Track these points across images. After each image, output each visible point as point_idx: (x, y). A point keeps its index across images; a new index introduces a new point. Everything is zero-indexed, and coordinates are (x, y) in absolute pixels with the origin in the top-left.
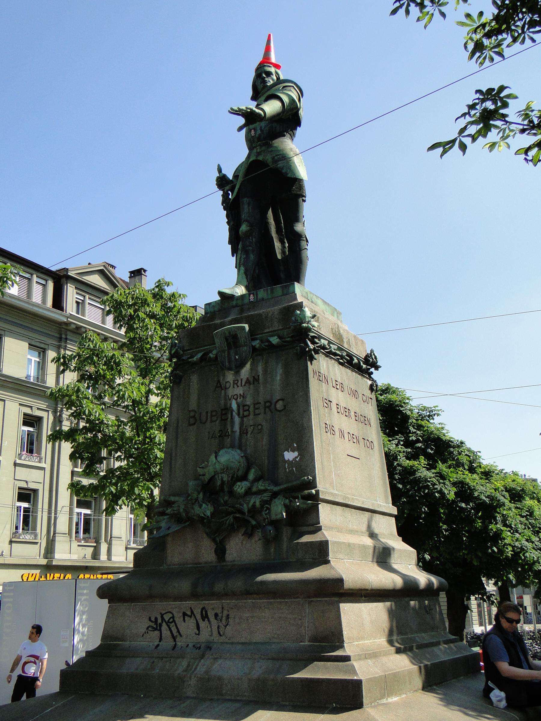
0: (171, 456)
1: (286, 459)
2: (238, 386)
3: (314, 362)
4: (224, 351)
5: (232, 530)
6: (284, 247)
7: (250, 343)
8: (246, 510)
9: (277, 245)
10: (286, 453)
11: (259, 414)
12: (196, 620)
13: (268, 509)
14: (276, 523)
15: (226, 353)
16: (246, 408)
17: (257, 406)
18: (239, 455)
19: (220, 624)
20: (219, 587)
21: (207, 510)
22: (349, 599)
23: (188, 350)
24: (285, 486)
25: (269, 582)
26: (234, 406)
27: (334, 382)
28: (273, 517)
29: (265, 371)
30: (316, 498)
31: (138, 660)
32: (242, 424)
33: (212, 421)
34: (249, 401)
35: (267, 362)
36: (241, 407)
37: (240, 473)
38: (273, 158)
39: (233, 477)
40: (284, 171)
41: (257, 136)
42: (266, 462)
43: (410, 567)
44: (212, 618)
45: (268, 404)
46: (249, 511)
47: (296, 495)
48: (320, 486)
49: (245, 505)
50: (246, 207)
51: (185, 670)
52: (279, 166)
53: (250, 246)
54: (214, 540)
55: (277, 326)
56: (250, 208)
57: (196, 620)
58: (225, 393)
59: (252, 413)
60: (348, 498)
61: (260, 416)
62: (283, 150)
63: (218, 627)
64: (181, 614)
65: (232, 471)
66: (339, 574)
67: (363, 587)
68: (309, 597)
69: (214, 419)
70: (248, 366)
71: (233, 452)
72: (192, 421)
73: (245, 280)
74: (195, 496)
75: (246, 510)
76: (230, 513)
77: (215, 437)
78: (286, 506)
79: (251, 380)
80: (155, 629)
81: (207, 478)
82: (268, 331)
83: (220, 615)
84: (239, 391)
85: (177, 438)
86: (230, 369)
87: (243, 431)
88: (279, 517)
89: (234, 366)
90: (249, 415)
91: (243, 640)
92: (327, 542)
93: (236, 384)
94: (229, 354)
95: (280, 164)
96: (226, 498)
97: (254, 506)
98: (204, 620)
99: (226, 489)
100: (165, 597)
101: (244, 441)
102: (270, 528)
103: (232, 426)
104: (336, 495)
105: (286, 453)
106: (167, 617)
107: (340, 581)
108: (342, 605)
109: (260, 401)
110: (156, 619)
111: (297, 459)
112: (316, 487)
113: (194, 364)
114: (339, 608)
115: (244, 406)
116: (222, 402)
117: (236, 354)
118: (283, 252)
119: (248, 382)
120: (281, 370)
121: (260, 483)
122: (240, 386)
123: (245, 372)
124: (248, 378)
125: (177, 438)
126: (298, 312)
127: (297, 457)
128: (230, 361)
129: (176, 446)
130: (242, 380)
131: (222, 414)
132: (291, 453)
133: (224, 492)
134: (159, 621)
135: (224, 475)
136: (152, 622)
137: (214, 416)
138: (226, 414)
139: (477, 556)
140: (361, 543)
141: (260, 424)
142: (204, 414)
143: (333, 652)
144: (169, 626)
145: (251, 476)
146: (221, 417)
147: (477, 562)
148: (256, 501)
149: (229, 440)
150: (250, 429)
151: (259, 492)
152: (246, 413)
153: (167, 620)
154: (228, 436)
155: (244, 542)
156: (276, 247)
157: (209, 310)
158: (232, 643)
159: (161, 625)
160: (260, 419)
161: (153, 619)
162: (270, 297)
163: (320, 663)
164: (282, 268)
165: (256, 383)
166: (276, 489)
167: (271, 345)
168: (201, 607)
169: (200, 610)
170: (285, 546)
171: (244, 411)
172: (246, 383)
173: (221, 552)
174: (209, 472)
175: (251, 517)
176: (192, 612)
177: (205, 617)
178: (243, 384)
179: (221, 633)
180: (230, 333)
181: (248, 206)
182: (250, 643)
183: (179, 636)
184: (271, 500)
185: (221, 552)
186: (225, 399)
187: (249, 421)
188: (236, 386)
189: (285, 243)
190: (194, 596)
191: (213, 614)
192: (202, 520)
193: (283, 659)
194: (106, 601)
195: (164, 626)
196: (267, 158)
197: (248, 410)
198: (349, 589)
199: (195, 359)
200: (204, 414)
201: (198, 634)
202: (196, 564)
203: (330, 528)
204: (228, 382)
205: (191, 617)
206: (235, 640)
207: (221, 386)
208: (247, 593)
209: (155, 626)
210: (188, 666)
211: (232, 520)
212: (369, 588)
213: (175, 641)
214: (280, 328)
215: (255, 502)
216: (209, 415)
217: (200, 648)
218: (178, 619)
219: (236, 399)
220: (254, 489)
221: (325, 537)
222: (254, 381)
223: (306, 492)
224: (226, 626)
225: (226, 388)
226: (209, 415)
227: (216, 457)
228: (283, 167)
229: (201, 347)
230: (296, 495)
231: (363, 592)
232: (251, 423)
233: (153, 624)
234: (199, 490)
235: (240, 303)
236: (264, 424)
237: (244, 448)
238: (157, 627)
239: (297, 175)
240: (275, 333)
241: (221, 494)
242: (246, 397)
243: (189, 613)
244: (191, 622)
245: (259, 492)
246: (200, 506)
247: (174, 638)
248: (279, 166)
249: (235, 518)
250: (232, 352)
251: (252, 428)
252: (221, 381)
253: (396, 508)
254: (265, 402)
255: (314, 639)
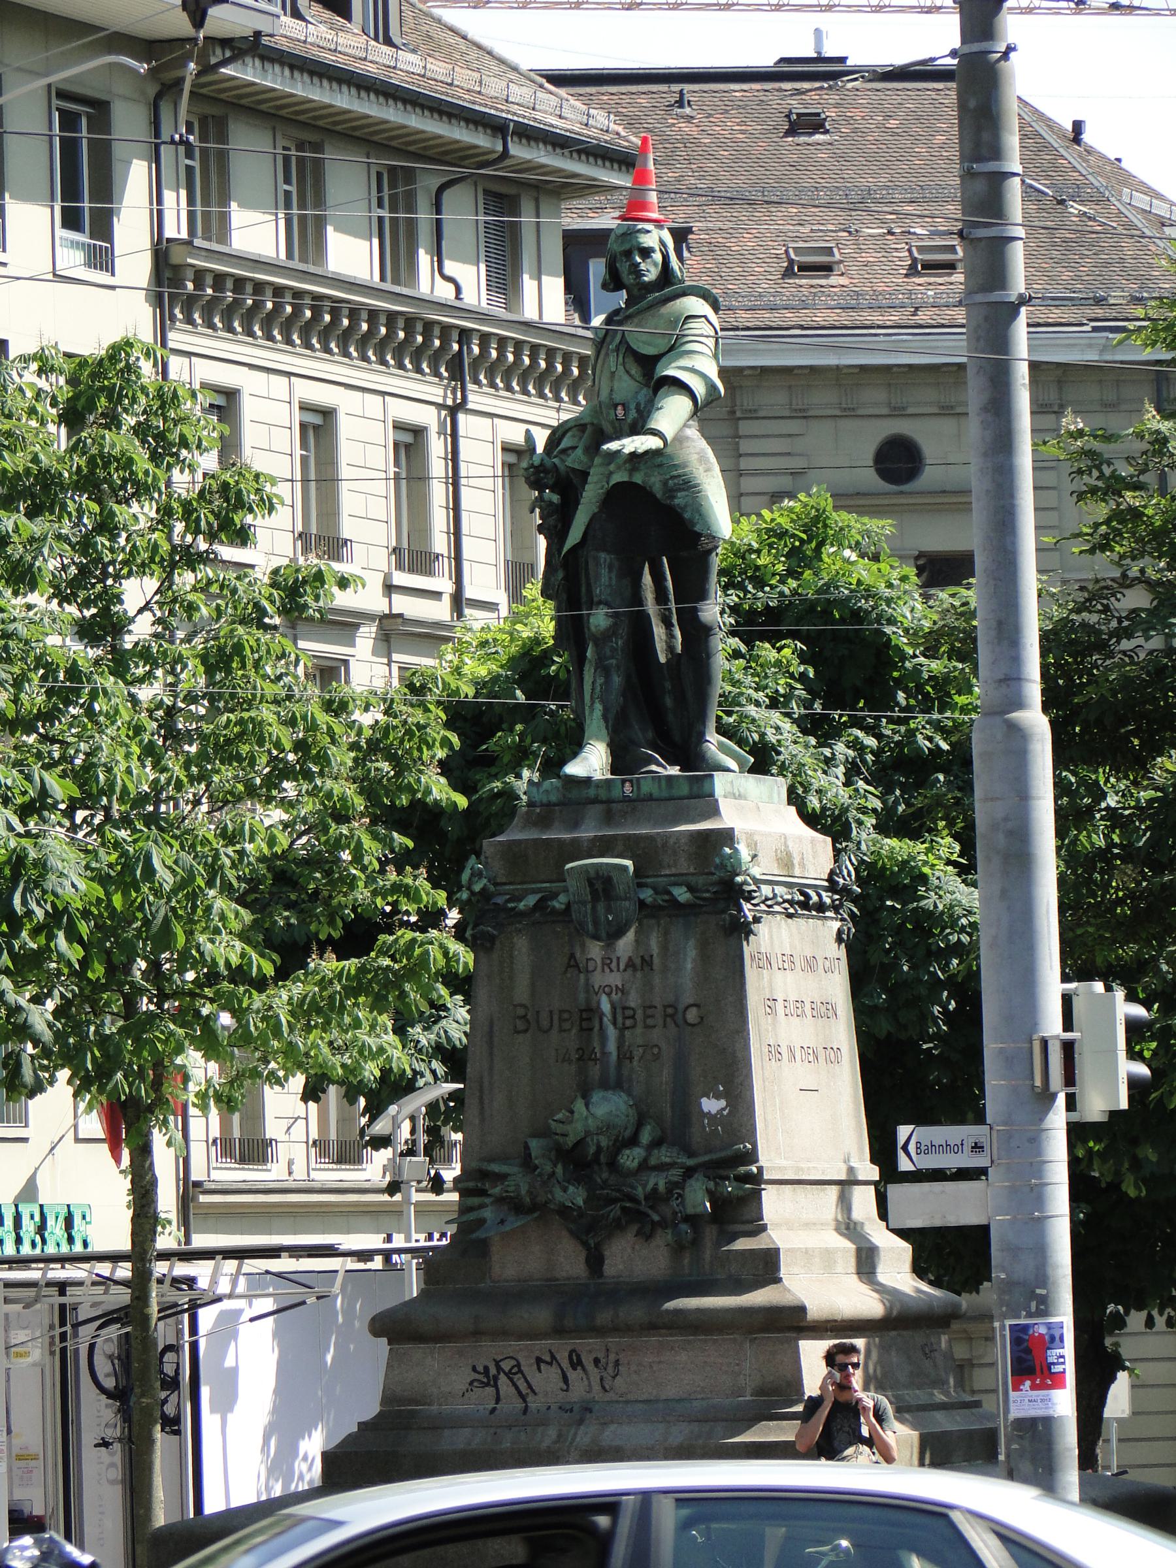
0: (481, 1087)
1: (706, 1110)
2: (611, 971)
3: (752, 938)
4: (584, 903)
5: (618, 1226)
6: (671, 636)
7: (636, 893)
8: (641, 1196)
9: (659, 631)
10: (704, 1101)
11: (654, 1027)
12: (562, 1370)
13: (680, 1195)
14: (694, 1220)
15: (589, 906)
16: (629, 1013)
17: (649, 1012)
18: (625, 1102)
19: (605, 1374)
20: (604, 1317)
21: (577, 1196)
22: (814, 1334)
23: (505, 884)
24: (706, 1158)
25: (689, 1310)
26: (606, 1006)
27: (779, 956)
28: (690, 1211)
29: (664, 948)
30: (757, 1179)
31: (467, 1431)
32: (621, 1040)
33: (561, 1030)
34: (633, 1001)
35: (666, 933)
36: (619, 1011)
37: (628, 1133)
38: (665, 483)
39: (616, 1140)
40: (687, 515)
41: (629, 421)
42: (669, 1114)
43: (899, 1276)
44: (590, 1367)
45: (670, 1011)
46: (646, 1198)
47: (723, 1173)
48: (764, 1159)
49: (640, 1189)
50: (604, 572)
51: (555, 1442)
52: (676, 501)
53: (612, 657)
54: (585, 1244)
55: (684, 866)
56: (613, 576)
57: (562, 1370)
58: (587, 980)
59: (640, 1025)
60: (802, 1169)
61: (656, 1031)
62: (684, 465)
63: (602, 1379)
64: (533, 1361)
65: (615, 1132)
66: (799, 1299)
67: (831, 1318)
68: (751, 1333)
69: (566, 1026)
70: (630, 935)
71: (615, 1098)
72: (521, 1025)
73: (604, 732)
74: (548, 1168)
75: (641, 1196)
76: (614, 1201)
77: (570, 1061)
78: (709, 1191)
79: (638, 961)
80: (487, 1384)
81: (570, 1141)
82: (667, 872)
83: (603, 1361)
84: (614, 979)
85: (491, 1054)
86: (596, 937)
87: (625, 1055)
88: (699, 1210)
89: (604, 935)
90: (634, 1027)
91: (644, 1397)
92: (777, 1250)
93: (609, 965)
94: (594, 909)
95: (680, 500)
96: (605, 1175)
97: (655, 1189)
98: (575, 1369)
99: (603, 1159)
100: (503, 1334)
101: (625, 1072)
102: (684, 1227)
103: (603, 1043)
104: (785, 1168)
105: (704, 1101)
106: (506, 1365)
107: (801, 1310)
108: (802, 1343)
109: (654, 1003)
110: (486, 1368)
111: (725, 1113)
112: (757, 1161)
113: (522, 914)
114: (797, 1347)
115: (624, 1008)
116: (582, 996)
117: (609, 910)
118: (670, 648)
119: (630, 964)
120: (694, 952)
121: (663, 1149)
122: (615, 969)
123: (626, 944)
124: (630, 959)
125: (491, 1054)
126: (727, 850)
127: (723, 1109)
128: (596, 923)
129: (491, 1069)
130: (618, 959)
131: (582, 1020)
132: (714, 1100)
133: (599, 1164)
134: (493, 1371)
135: (602, 1138)
136: (479, 1373)
137: (567, 1020)
138: (589, 1019)
139: (1137, 1164)
140: (823, 1245)
141: (657, 1046)
142: (544, 1015)
143: (738, 1435)
144: (511, 1380)
145: (645, 1137)
146: (581, 1025)
147: (1137, 1187)
148: (659, 1181)
149: (598, 1066)
150: (637, 1053)
151: (661, 1168)
152: (628, 1023)
153: (507, 1370)
154: (596, 1060)
155: (637, 1247)
156: (656, 637)
157: (537, 798)
158: (627, 1402)
159: (496, 1378)
160: (656, 1035)
161: (480, 1369)
162: (665, 794)
163: (771, 1423)
164: (668, 685)
165: (646, 969)
166: (691, 1162)
167: (674, 902)
168: (569, 1348)
169: (567, 1354)
170: (707, 1255)
171: (625, 1018)
172: (627, 966)
173: (595, 1261)
174: (575, 1130)
175: (651, 1207)
176: (553, 1357)
177: (576, 1362)
178: (622, 967)
179: (607, 1387)
180: (597, 873)
181: (610, 571)
182: (657, 1401)
183: (531, 1394)
184: (684, 1181)
185: (595, 1261)
186: (587, 992)
187: (636, 1036)
188: (606, 969)
189: (673, 625)
190: (559, 1331)
191: (591, 1359)
192: (564, 1211)
193: (716, 1420)
194: (385, 1340)
195: (503, 1380)
196: (653, 479)
197: (633, 1017)
198: (814, 1321)
199: (522, 906)
200: (544, 1015)
201: (567, 1390)
202: (548, 1280)
203: (778, 1225)
204: (592, 959)
205: (550, 1364)
206: (631, 1397)
207: (577, 966)
208: (652, 1327)
209: (485, 1380)
210: (560, 1436)
211: (619, 1213)
212: (839, 1318)
213: (525, 1401)
214: (692, 870)
215: (656, 1184)
216: (556, 1017)
217: (571, 1410)
218: (529, 1368)
219: (609, 995)
220: (653, 1161)
221: (774, 1242)
222: (641, 964)
223: (742, 1169)
224: (614, 1377)
225: (587, 971)
226: (556, 1017)
227: (587, 1105)
228: (686, 506)
229: (534, 882)
230: (723, 1173)
231: (829, 1326)
232: (640, 1041)
233: (481, 1377)
234: (553, 1158)
235: (603, 794)
236: (664, 1046)
237: (626, 1086)
238: (492, 1382)
239: (714, 528)
240: (681, 879)
241: (596, 1168)
242: (628, 993)
243: (548, 1359)
244: (552, 1373)
245: (661, 1168)
246: (565, 1190)
247: (523, 1397)
248: (676, 501)
249: (623, 1209)
250: (601, 907)
251: (641, 1050)
252: (578, 955)
253: (877, 1168)
254: (665, 1007)
255: (760, 1392)
